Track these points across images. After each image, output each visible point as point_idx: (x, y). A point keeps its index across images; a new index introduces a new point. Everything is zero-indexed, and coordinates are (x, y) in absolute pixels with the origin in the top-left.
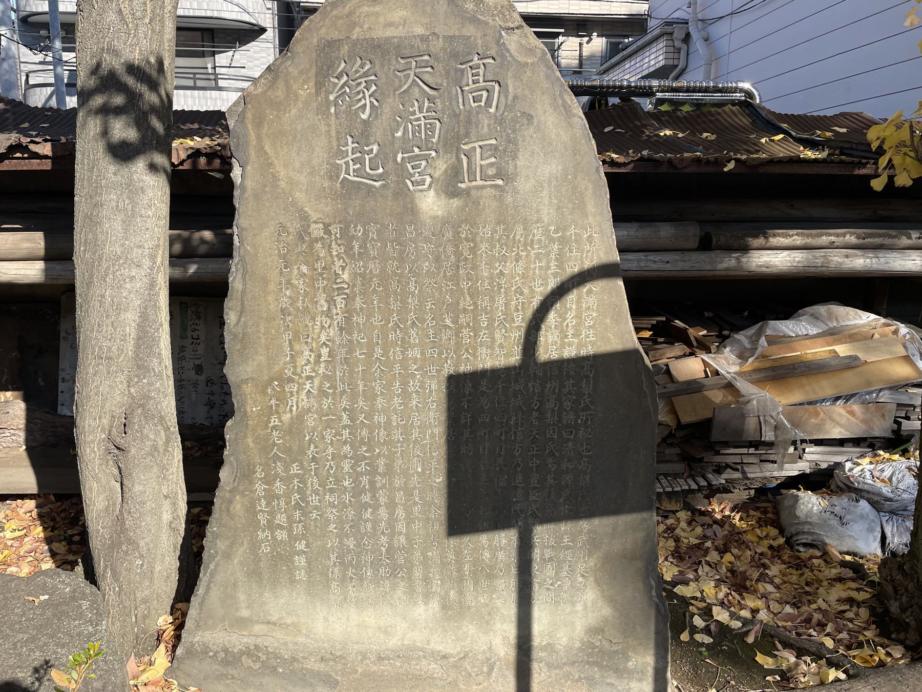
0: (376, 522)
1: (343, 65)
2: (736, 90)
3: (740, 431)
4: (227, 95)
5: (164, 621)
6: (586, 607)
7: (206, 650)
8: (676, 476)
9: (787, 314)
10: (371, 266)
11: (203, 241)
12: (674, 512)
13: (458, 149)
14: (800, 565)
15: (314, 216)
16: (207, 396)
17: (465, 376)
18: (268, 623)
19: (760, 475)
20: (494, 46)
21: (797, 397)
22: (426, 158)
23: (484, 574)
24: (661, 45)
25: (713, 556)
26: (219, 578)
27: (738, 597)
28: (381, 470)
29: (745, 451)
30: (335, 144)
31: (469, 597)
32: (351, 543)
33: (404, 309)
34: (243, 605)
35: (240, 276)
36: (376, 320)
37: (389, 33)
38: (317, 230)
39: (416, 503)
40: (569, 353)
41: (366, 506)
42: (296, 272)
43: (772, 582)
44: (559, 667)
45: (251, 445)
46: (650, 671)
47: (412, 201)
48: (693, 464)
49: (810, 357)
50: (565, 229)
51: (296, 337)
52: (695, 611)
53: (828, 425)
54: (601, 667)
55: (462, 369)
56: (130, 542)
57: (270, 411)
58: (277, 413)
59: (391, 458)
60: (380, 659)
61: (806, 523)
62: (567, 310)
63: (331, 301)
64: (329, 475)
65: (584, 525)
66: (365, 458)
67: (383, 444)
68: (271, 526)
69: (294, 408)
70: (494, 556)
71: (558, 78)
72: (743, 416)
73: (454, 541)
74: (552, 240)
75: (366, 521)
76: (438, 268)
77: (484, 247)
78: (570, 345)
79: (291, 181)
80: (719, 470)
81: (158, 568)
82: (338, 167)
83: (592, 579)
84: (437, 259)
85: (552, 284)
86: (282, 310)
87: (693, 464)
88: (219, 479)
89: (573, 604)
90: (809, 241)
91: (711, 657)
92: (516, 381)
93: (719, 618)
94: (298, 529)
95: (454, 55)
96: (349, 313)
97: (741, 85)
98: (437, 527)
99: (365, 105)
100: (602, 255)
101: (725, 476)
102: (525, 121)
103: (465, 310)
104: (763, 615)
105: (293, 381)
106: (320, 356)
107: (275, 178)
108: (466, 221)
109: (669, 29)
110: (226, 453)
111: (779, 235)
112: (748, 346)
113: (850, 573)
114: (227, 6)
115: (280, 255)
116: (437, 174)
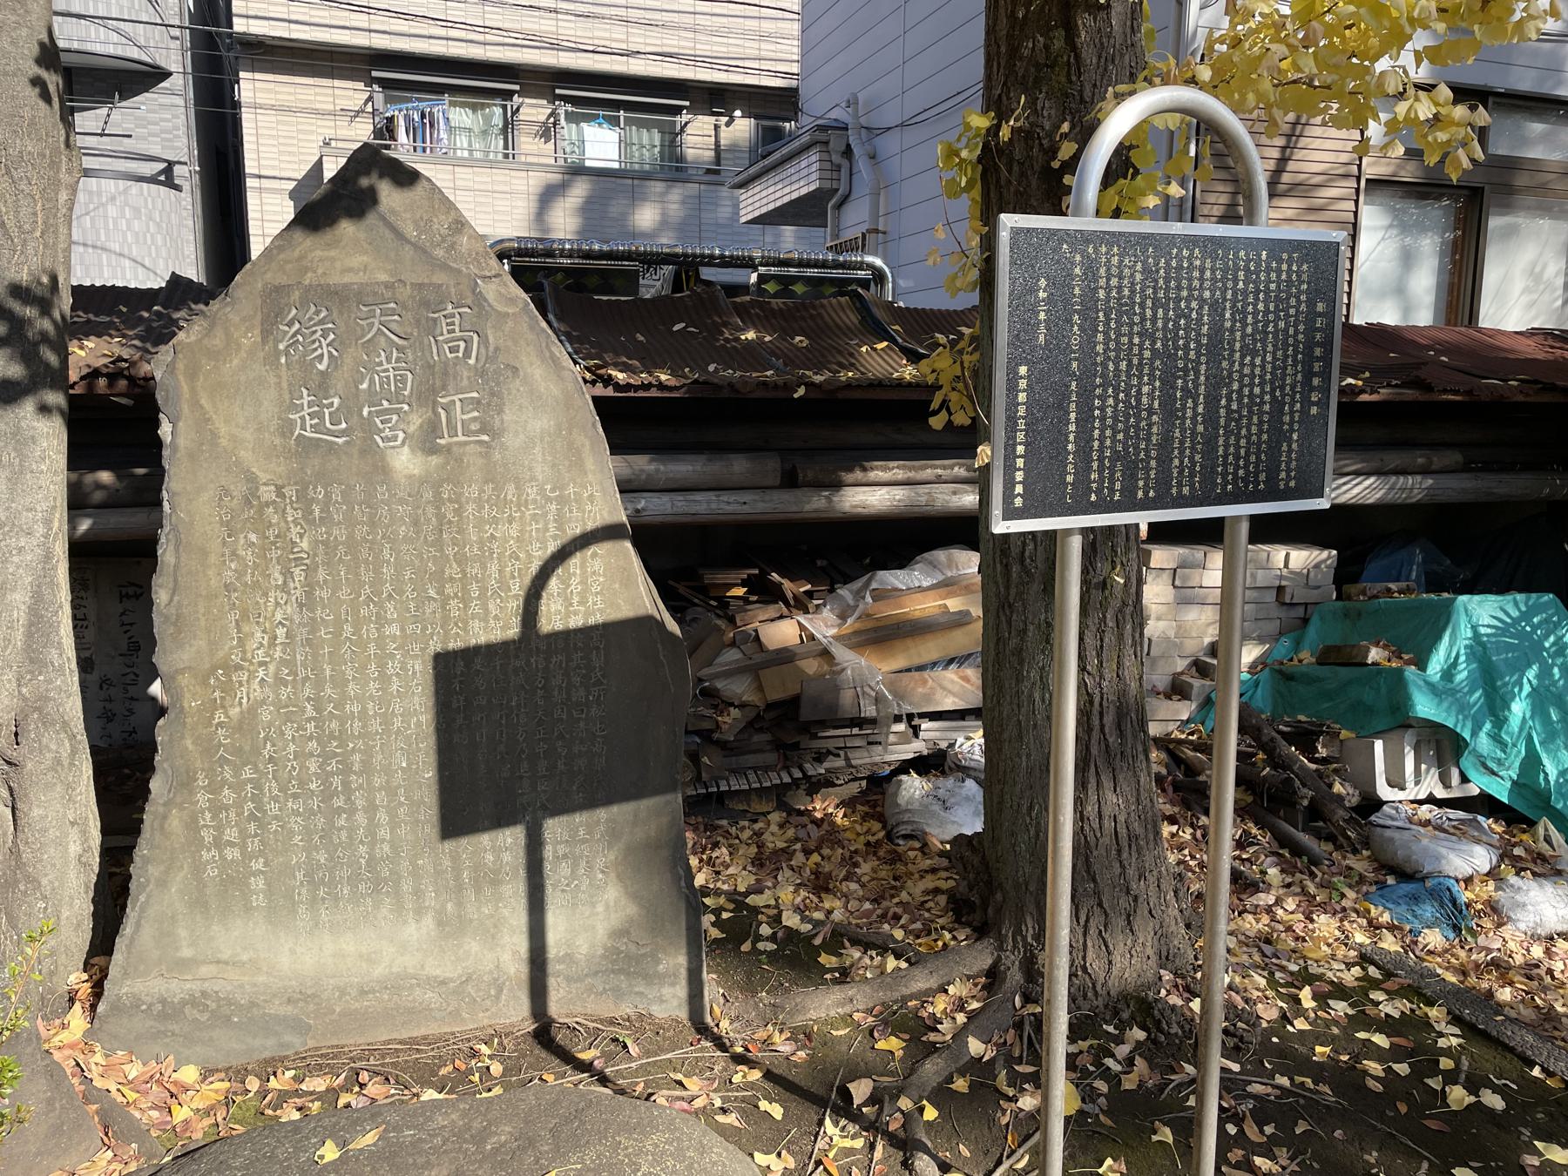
0: (351, 830)
1: (294, 311)
2: (861, 266)
3: (834, 707)
4: (99, 185)
5: (77, 979)
6: (607, 907)
7: (136, 1003)
8: (767, 769)
9: (902, 561)
10: (336, 532)
11: (99, 486)
12: (765, 814)
13: (435, 403)
14: (896, 858)
15: (263, 477)
16: (102, 704)
17: (455, 654)
18: (218, 962)
19: (868, 760)
20: (469, 294)
21: (900, 662)
22: (398, 412)
23: (489, 879)
24: (814, 158)
25: (799, 858)
26: (151, 912)
27: (815, 900)
28: (356, 767)
29: (847, 731)
30: (287, 397)
31: (471, 910)
32: (322, 857)
33: (377, 582)
34: (184, 943)
35: (171, 547)
36: (344, 594)
37: (347, 279)
38: (268, 493)
39: (401, 804)
40: (576, 622)
41: (339, 811)
42: (242, 541)
43: (858, 881)
44: (579, 980)
45: (191, 747)
46: (683, 973)
47: (383, 459)
48: (788, 752)
49: (917, 614)
50: (563, 488)
51: (245, 616)
52: (764, 918)
53: (939, 694)
54: (628, 974)
55: (451, 646)
56: (29, 879)
57: (213, 706)
58: (223, 707)
59: (368, 753)
60: (363, 993)
61: (908, 811)
62: (570, 576)
63: (287, 574)
64: (291, 777)
65: (602, 814)
66: (336, 755)
67: (359, 737)
68: (218, 844)
69: (245, 701)
70: (498, 858)
71: (543, 330)
72: (837, 689)
73: (449, 845)
74: (549, 500)
75: (339, 829)
76: (417, 533)
77: (470, 508)
78: (576, 613)
79: (233, 438)
80: (819, 758)
81: (65, 913)
82: (292, 423)
83: (613, 875)
84: (416, 523)
85: (552, 547)
86: (226, 586)
87: (788, 752)
88: (149, 791)
89: (593, 905)
90: (911, 474)
91: (770, 963)
92: (517, 657)
93: (789, 924)
94: (253, 845)
95: (426, 304)
96: (310, 586)
97: (869, 259)
98: (428, 830)
99: (322, 355)
100: (605, 514)
101: (826, 765)
102: (509, 373)
103: (451, 579)
104: (837, 916)
105: (241, 668)
106: (275, 638)
107: (215, 435)
108: (448, 480)
109: (822, 136)
110: (157, 758)
111: (877, 468)
112: (851, 603)
113: (945, 862)
114: (97, 32)
115: (222, 523)
116: (412, 429)
